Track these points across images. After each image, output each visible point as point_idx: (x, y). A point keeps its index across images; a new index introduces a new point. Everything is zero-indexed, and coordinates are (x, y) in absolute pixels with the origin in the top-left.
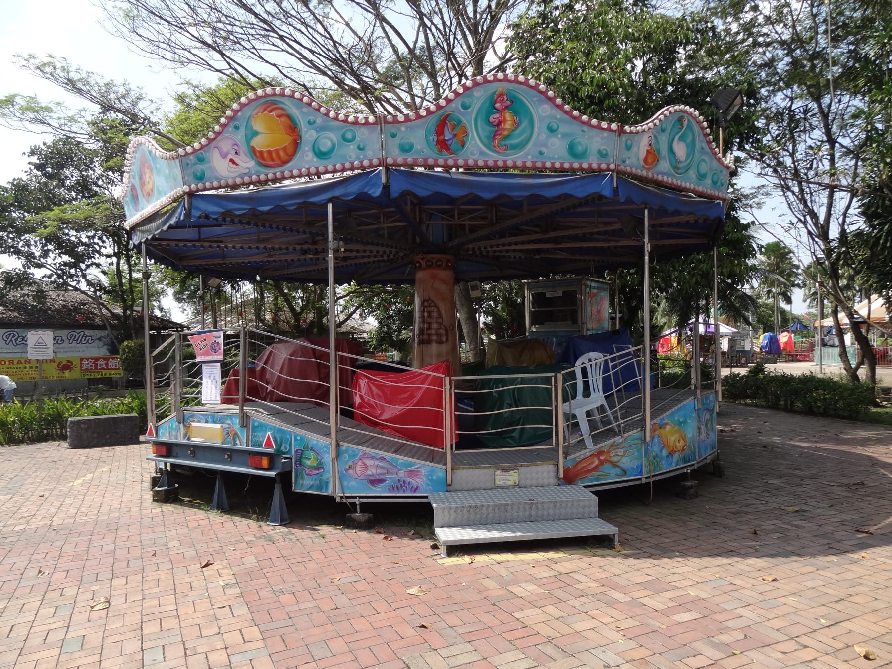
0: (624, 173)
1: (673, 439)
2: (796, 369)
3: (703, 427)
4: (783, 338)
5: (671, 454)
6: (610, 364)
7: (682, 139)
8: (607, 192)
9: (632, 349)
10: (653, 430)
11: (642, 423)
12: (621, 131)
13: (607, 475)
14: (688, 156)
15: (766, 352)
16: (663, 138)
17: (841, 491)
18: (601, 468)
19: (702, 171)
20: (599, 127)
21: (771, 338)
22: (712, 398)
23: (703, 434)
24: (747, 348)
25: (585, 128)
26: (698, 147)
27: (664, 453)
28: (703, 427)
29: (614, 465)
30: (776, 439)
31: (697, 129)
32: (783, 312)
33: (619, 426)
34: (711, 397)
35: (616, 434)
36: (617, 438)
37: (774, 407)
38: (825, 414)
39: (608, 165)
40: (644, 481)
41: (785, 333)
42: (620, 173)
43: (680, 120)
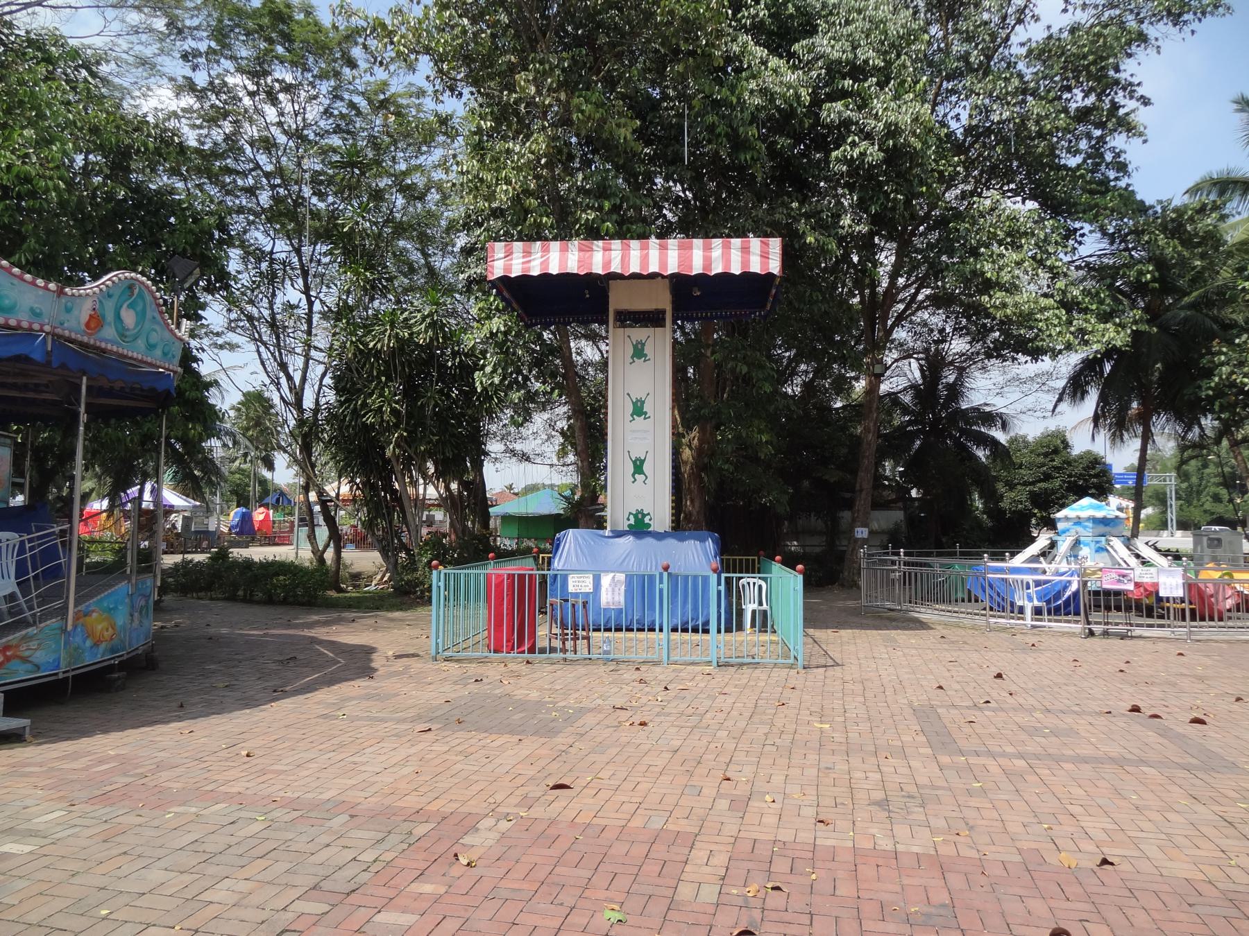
0: (60, 337)
1: (100, 627)
2: (258, 553)
3: (136, 614)
4: (259, 515)
5: (96, 645)
6: (28, 546)
7: (131, 306)
8: (37, 356)
9: (57, 529)
10: (76, 619)
11: (63, 611)
12: (60, 292)
13: (15, 672)
14: (137, 324)
15: (237, 533)
16: (109, 306)
17: (274, 666)
18: (8, 665)
19: (152, 341)
20: (33, 284)
21: (244, 515)
22: (149, 583)
23: (136, 622)
24: (212, 528)
25: (16, 281)
26: (149, 314)
27: (88, 643)
28: (136, 614)
29: (25, 660)
30: (224, 631)
31: (148, 298)
32: (263, 482)
33: (34, 615)
34: (149, 583)
35: (28, 625)
36: (30, 630)
37: (232, 598)
38: (284, 602)
39: (42, 326)
40: (61, 676)
41: (262, 510)
42: (57, 337)
43: (131, 288)
